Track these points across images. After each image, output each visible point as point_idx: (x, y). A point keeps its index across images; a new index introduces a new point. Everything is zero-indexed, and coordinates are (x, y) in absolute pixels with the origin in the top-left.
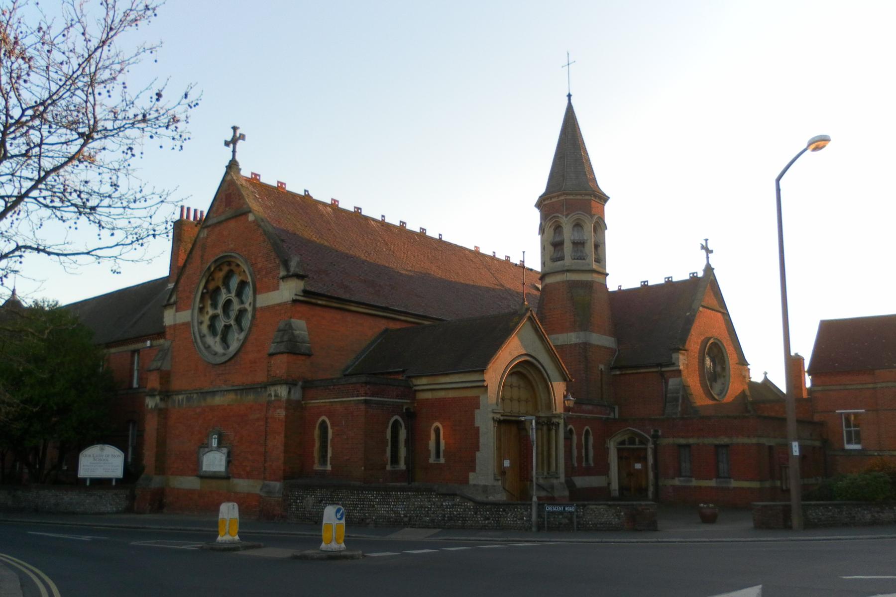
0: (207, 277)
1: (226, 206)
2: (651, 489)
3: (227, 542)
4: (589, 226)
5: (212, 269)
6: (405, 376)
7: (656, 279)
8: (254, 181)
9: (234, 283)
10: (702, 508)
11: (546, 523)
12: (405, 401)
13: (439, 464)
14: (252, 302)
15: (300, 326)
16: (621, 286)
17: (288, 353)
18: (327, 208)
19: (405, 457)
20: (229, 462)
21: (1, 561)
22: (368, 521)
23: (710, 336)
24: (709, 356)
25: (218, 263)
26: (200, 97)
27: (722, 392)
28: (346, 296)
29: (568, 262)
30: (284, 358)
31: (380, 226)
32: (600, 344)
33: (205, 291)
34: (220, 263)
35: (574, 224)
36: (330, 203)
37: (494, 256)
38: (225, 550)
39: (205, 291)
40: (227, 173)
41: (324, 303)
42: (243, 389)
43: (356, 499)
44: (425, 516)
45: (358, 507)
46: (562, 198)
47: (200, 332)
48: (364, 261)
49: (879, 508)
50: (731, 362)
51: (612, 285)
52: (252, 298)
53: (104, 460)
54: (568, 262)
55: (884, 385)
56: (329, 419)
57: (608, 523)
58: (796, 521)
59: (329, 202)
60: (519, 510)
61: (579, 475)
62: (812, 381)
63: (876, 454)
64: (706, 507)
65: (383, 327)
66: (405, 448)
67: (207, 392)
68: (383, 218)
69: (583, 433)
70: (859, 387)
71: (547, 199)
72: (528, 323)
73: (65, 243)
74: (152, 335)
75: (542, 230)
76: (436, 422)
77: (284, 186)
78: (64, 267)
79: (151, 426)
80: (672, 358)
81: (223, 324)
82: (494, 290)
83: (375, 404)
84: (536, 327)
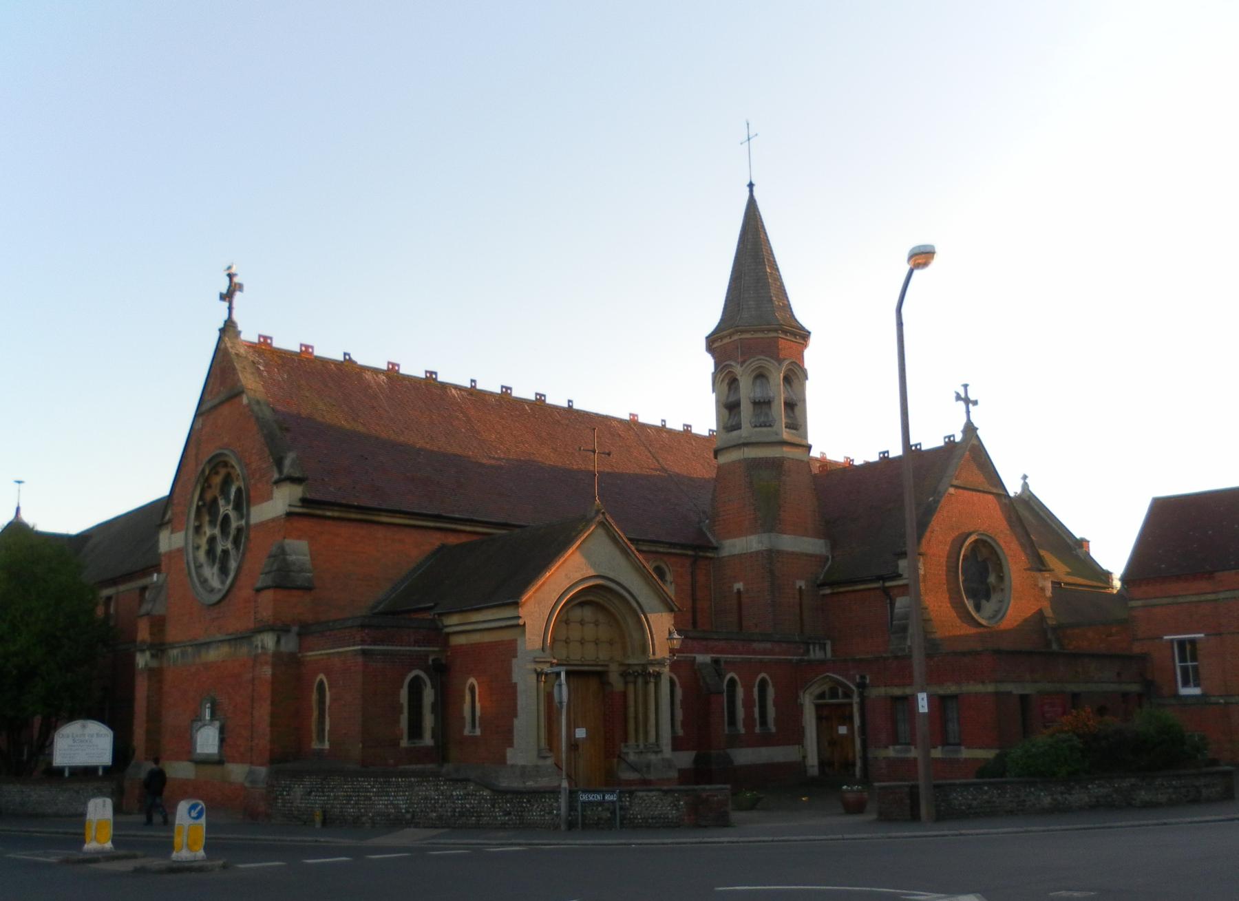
2: (859, 763)
4: (777, 377)
5: (207, 472)
6: (432, 613)
8: (263, 347)
12: (431, 649)
15: (299, 549)
18: (380, 376)
20: (222, 741)
22: (364, 819)
27: (997, 614)
28: (374, 504)
29: (746, 431)
32: (796, 549)
35: (726, 381)
39: (200, 503)
40: (220, 338)
41: (336, 514)
44: (432, 811)
45: (352, 800)
46: (735, 337)
49: (1063, 788)
53: (87, 741)
54: (746, 431)
55: (1228, 594)
56: (327, 678)
57: (662, 816)
59: (384, 367)
60: (547, 800)
63: (1222, 701)
65: (437, 543)
68: (663, 423)
69: (754, 684)
70: (1195, 599)
71: (721, 339)
80: (897, 566)
84: (615, 536)
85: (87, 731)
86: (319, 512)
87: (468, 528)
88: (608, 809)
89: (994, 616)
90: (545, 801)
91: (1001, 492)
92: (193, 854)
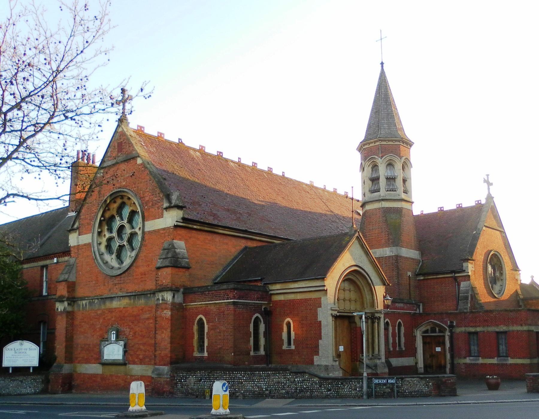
1: (118, 152)
2: (448, 366)
3: (137, 411)
4: (398, 166)
5: (108, 202)
6: (263, 283)
7: (449, 206)
8: (140, 131)
9: (126, 212)
10: (488, 379)
14: (141, 227)
15: (181, 246)
16: (423, 211)
19: (264, 345)
20: (125, 352)
24: (491, 264)
25: (113, 197)
26: (152, 91)
27: (500, 292)
28: (216, 222)
29: (383, 193)
30: (169, 270)
31: (237, 166)
33: (102, 219)
34: (114, 197)
36: (198, 149)
41: (198, 227)
43: (228, 378)
44: (282, 390)
46: (377, 144)
48: (227, 194)
52: (141, 225)
54: (383, 193)
60: (353, 383)
61: (394, 357)
64: (492, 378)
65: (243, 246)
66: (264, 338)
67: (106, 298)
71: (366, 144)
72: (356, 241)
73: (42, 192)
74: (59, 253)
76: (287, 318)
77: (163, 136)
78: (39, 208)
79: (61, 325)
80: (463, 266)
81: (118, 244)
82: (326, 215)
86: (190, 226)
87: (258, 238)
88: (389, 388)
89: (500, 293)
90: (352, 383)
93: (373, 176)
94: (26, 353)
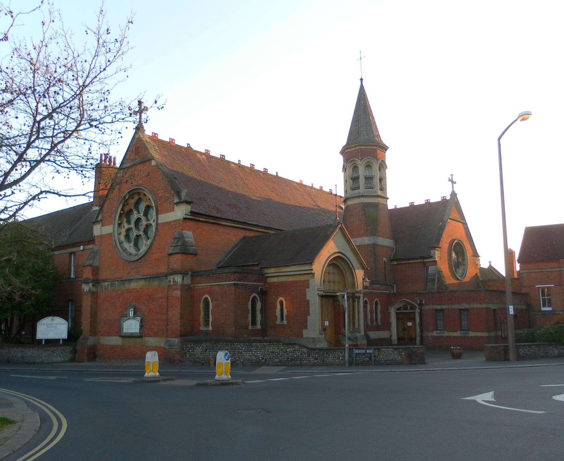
0: (124, 203)
1: (136, 155)
2: (418, 339)
3: (152, 377)
4: (376, 167)
8: (154, 138)
9: (142, 207)
10: (452, 349)
11: (354, 360)
13: (283, 324)
14: (155, 219)
15: (189, 235)
16: (396, 206)
17: (181, 253)
20: (141, 326)
21: (1, 392)
23: (455, 238)
24: (454, 251)
25: (131, 194)
27: (463, 275)
28: (219, 215)
29: (362, 190)
32: (383, 244)
33: (122, 212)
34: (132, 194)
37: (313, 186)
38: (151, 382)
40: (136, 133)
41: (204, 220)
42: (150, 278)
43: (230, 348)
47: (119, 239)
48: (229, 191)
50: (468, 255)
51: (391, 205)
52: (155, 217)
54: (362, 190)
58: (512, 355)
59: (204, 152)
60: (337, 353)
62: (520, 266)
64: (456, 349)
65: (243, 235)
70: (550, 270)
71: (348, 149)
72: (340, 232)
75: (345, 169)
79: (86, 304)
80: (430, 253)
81: (135, 234)
82: (313, 209)
83: (240, 286)
85: (54, 322)
89: (462, 276)
91: (465, 222)
92: (227, 376)
93: (354, 176)
94: (56, 327)
